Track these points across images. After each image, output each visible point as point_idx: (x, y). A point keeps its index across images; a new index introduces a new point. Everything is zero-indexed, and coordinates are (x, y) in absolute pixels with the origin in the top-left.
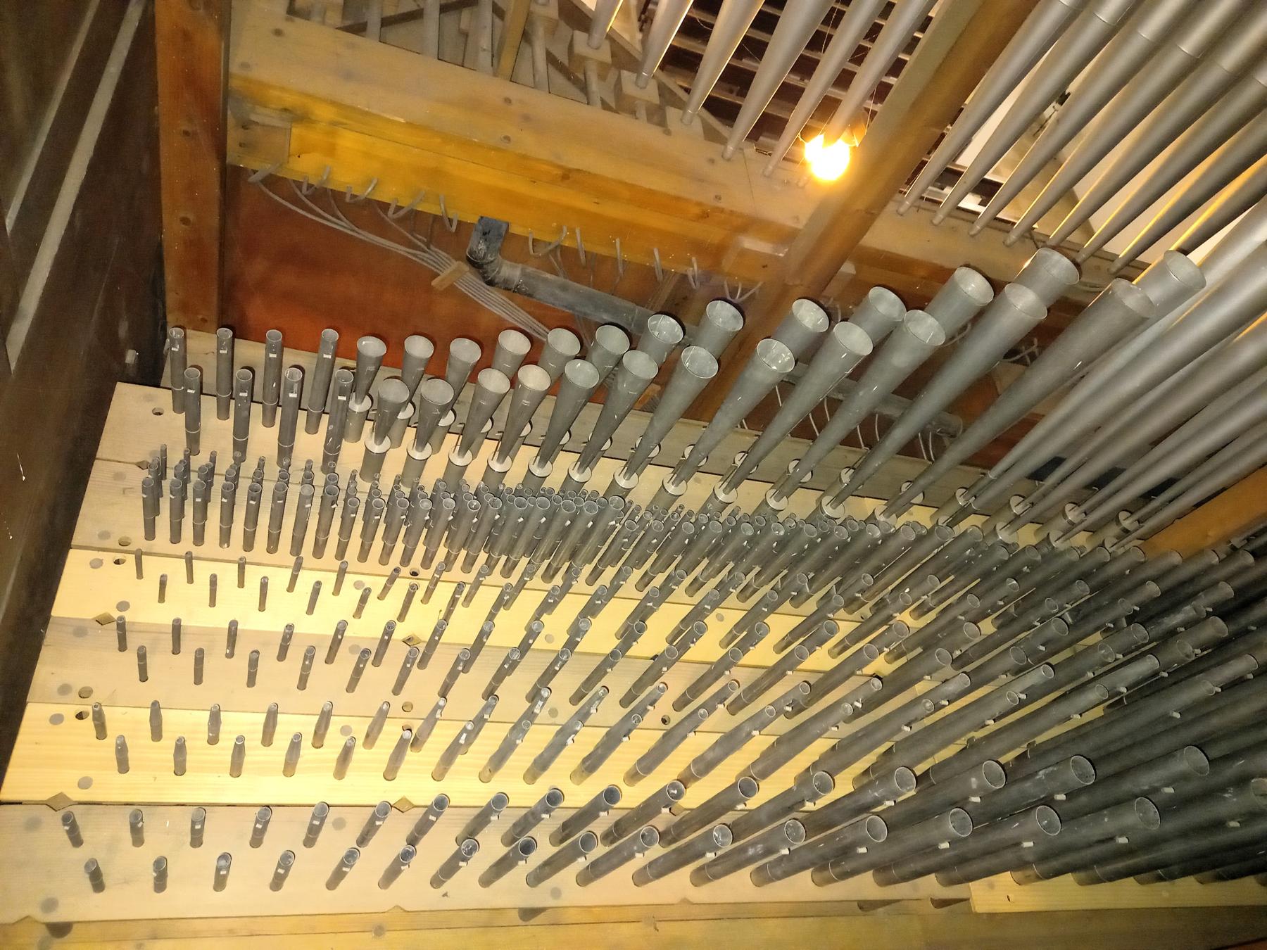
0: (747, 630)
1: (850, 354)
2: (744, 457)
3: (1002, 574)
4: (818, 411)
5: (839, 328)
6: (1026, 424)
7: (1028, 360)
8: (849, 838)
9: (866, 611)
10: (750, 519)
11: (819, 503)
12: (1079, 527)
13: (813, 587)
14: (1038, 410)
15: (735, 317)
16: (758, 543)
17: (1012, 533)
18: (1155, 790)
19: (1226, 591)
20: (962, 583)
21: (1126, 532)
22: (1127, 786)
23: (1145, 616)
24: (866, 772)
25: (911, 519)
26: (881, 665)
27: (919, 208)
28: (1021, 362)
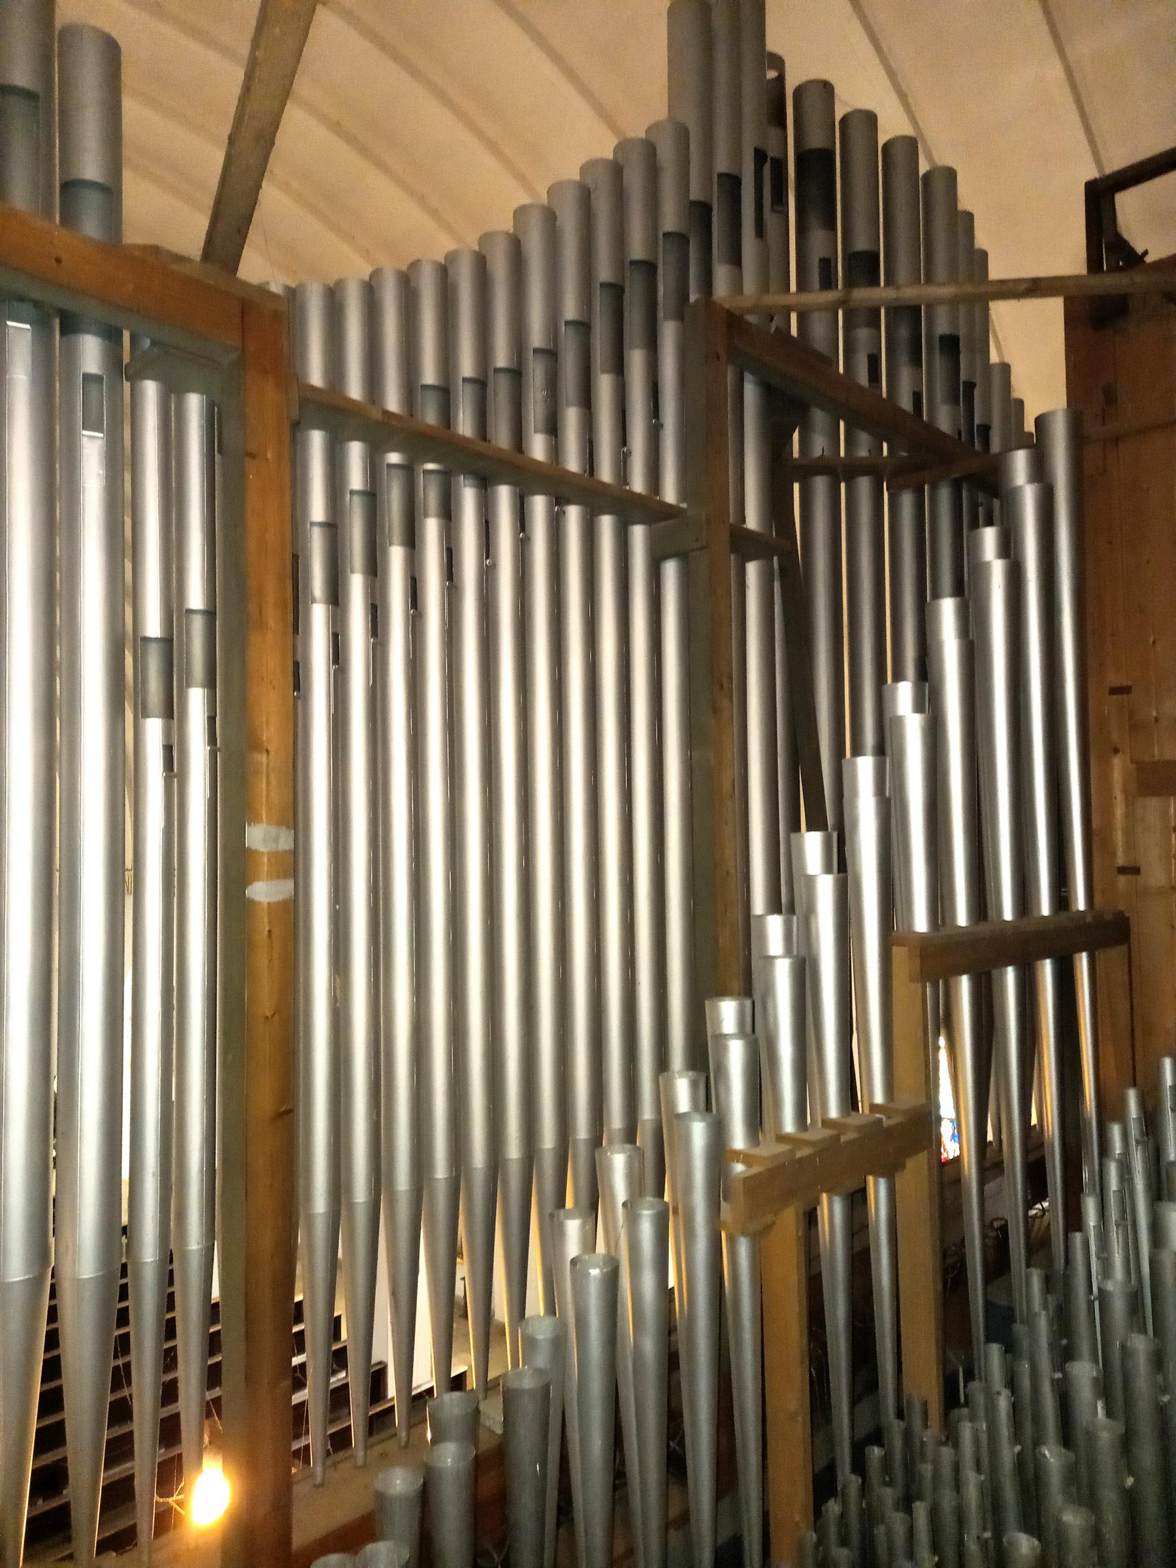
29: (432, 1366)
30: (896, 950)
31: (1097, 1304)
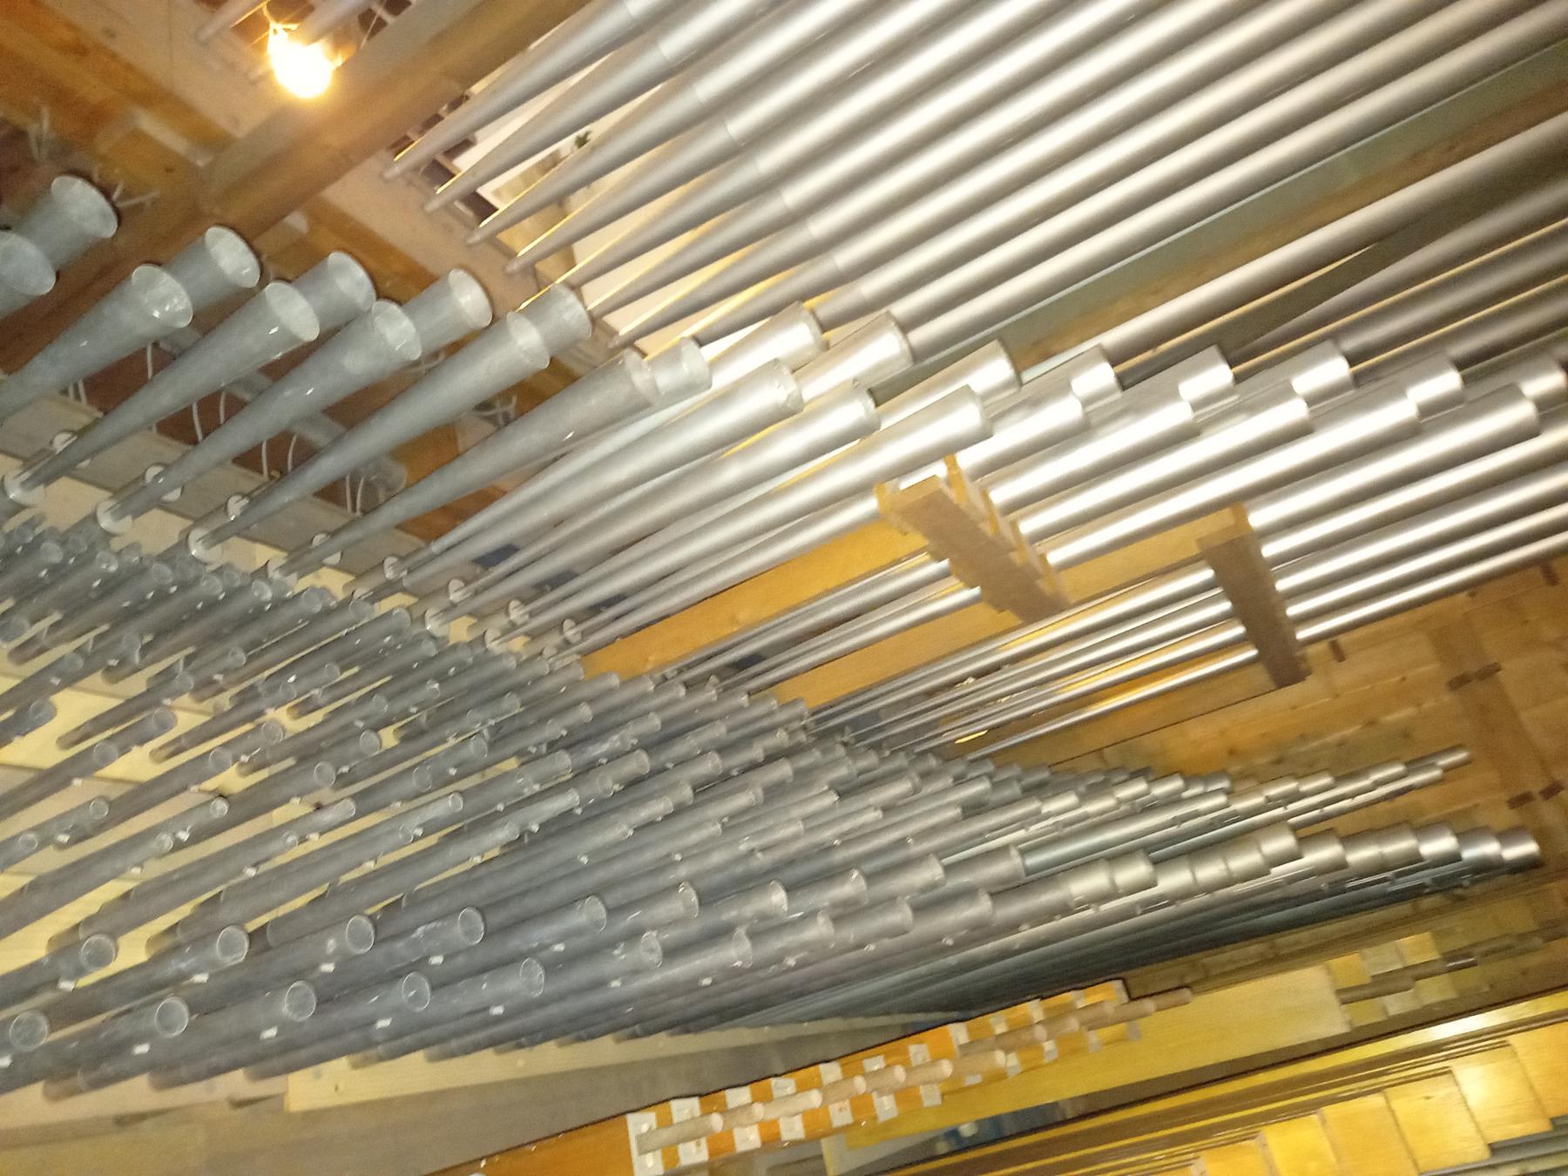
0: (16, 707)
1: (284, 330)
2: (70, 442)
3: (420, 675)
4: (209, 403)
5: (274, 290)
6: (484, 497)
7: (501, 421)
8: (124, 1028)
9: (225, 700)
10: (63, 539)
11: (185, 536)
12: (521, 630)
13: (148, 657)
14: (501, 483)
15: (104, 216)
16: (64, 577)
17: (445, 623)
18: (544, 947)
19: (655, 722)
20: (369, 677)
21: (567, 644)
22: (515, 943)
23: (572, 743)
24: (172, 930)
25: (319, 584)
26: (233, 780)
27: (410, 183)
28: (491, 419)
29: (1053, 539)
30: (1226, 512)
31: (971, 757)
